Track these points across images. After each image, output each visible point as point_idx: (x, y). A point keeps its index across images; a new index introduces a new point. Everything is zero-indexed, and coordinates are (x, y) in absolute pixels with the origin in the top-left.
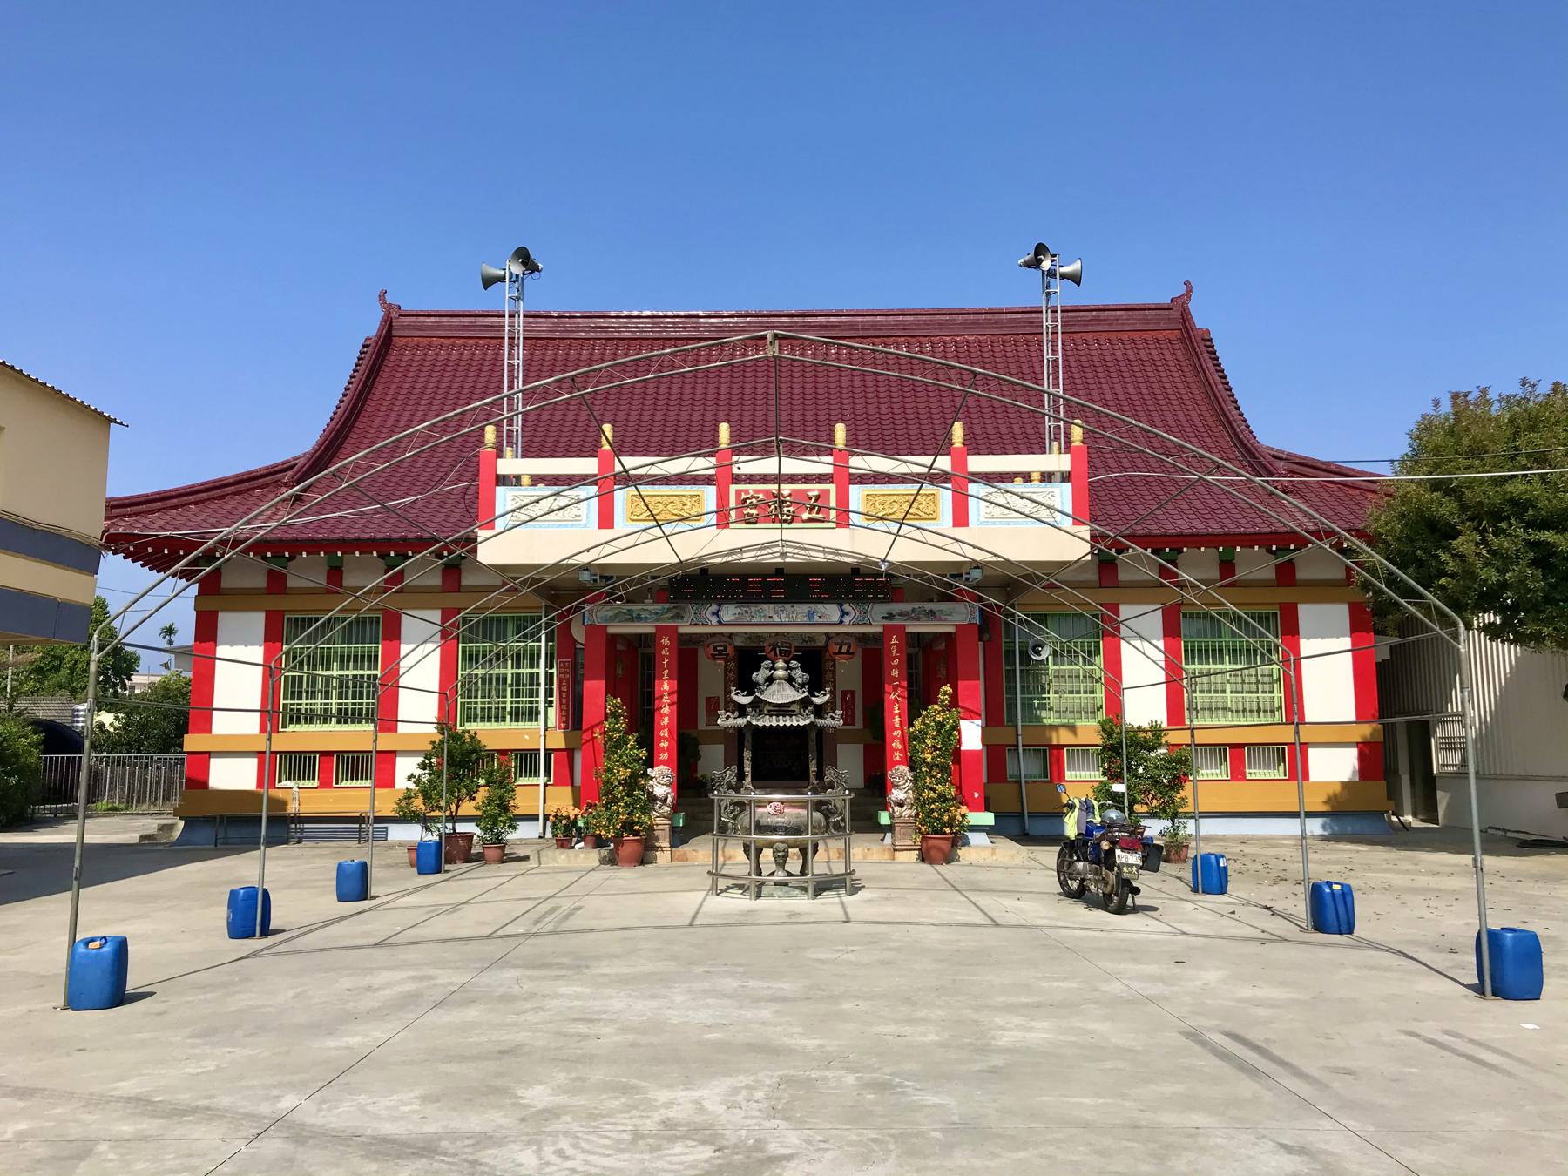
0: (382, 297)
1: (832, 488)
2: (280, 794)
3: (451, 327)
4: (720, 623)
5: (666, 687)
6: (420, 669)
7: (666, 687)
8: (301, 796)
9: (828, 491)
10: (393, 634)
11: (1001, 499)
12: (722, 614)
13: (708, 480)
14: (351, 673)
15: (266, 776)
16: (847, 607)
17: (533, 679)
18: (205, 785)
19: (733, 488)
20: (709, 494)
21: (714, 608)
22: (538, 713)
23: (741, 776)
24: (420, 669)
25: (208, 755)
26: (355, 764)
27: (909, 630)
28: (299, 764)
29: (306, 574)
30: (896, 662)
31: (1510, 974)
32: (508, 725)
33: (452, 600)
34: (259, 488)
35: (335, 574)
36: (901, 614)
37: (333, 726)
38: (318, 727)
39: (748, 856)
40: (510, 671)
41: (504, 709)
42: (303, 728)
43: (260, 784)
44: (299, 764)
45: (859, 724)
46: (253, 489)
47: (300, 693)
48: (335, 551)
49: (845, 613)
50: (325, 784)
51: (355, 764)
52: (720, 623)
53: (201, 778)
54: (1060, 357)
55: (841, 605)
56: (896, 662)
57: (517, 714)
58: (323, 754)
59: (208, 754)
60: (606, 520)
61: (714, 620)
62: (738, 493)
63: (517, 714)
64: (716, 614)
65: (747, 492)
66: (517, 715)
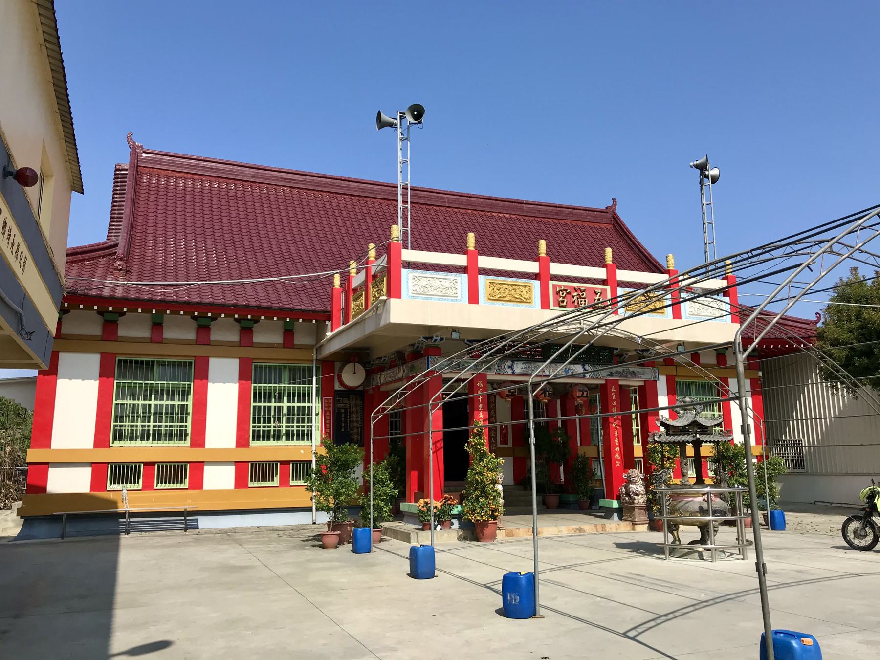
0: (129, 140)
1: (608, 288)
2: (111, 496)
3: (181, 165)
4: (514, 374)
5: (481, 416)
6: (223, 397)
7: (481, 416)
8: (128, 498)
9: (606, 290)
10: (203, 375)
11: (714, 304)
12: (515, 367)
13: (536, 276)
14: (296, 405)
15: (97, 482)
16: (587, 367)
17: (183, 408)
18: (44, 489)
19: (551, 283)
20: (536, 284)
21: (509, 363)
22: (186, 435)
23: (521, 479)
24: (223, 397)
25: (45, 466)
26: (172, 472)
27: (621, 383)
28: (124, 472)
29: (134, 328)
30: (615, 403)
31: (421, 570)
32: (283, 443)
33: (248, 353)
34: (88, 260)
35: (157, 326)
36: (617, 373)
37: (149, 443)
38: (272, 443)
39: (690, 543)
40: (285, 404)
41: (269, 431)
42: (127, 444)
43: (94, 487)
44: (124, 472)
45: (510, 444)
46: (84, 260)
47: (269, 419)
48: (158, 310)
49: (586, 371)
50: (148, 486)
51: (172, 472)
52: (514, 374)
53: (40, 483)
54: (409, 229)
55: (584, 366)
56: (615, 403)
57: (171, 435)
58: (146, 464)
59: (47, 465)
60: (473, 298)
61: (510, 371)
62: (554, 286)
63: (171, 435)
64: (511, 367)
65: (560, 286)
66: (289, 436)
